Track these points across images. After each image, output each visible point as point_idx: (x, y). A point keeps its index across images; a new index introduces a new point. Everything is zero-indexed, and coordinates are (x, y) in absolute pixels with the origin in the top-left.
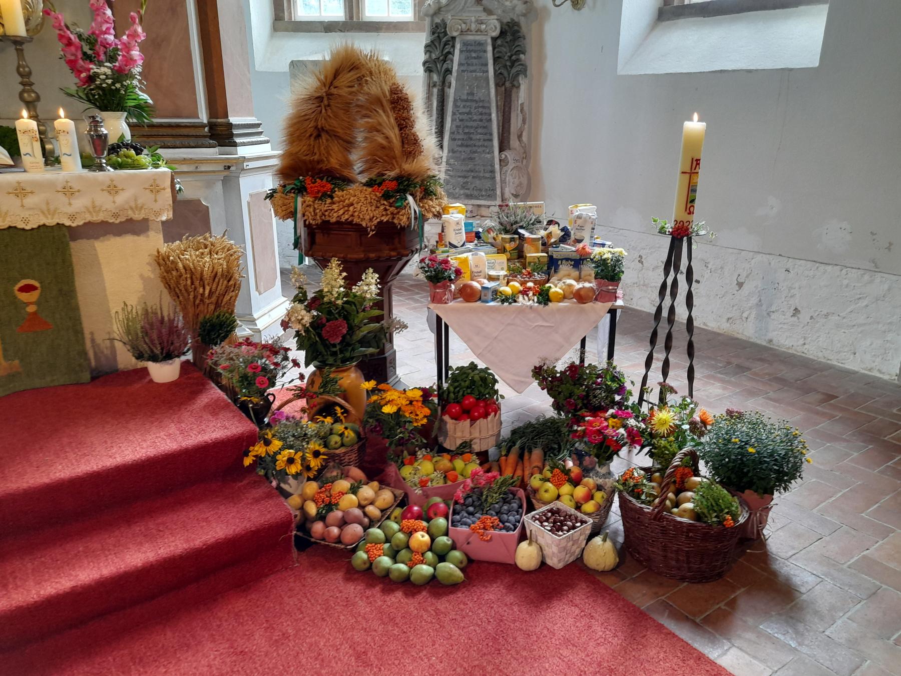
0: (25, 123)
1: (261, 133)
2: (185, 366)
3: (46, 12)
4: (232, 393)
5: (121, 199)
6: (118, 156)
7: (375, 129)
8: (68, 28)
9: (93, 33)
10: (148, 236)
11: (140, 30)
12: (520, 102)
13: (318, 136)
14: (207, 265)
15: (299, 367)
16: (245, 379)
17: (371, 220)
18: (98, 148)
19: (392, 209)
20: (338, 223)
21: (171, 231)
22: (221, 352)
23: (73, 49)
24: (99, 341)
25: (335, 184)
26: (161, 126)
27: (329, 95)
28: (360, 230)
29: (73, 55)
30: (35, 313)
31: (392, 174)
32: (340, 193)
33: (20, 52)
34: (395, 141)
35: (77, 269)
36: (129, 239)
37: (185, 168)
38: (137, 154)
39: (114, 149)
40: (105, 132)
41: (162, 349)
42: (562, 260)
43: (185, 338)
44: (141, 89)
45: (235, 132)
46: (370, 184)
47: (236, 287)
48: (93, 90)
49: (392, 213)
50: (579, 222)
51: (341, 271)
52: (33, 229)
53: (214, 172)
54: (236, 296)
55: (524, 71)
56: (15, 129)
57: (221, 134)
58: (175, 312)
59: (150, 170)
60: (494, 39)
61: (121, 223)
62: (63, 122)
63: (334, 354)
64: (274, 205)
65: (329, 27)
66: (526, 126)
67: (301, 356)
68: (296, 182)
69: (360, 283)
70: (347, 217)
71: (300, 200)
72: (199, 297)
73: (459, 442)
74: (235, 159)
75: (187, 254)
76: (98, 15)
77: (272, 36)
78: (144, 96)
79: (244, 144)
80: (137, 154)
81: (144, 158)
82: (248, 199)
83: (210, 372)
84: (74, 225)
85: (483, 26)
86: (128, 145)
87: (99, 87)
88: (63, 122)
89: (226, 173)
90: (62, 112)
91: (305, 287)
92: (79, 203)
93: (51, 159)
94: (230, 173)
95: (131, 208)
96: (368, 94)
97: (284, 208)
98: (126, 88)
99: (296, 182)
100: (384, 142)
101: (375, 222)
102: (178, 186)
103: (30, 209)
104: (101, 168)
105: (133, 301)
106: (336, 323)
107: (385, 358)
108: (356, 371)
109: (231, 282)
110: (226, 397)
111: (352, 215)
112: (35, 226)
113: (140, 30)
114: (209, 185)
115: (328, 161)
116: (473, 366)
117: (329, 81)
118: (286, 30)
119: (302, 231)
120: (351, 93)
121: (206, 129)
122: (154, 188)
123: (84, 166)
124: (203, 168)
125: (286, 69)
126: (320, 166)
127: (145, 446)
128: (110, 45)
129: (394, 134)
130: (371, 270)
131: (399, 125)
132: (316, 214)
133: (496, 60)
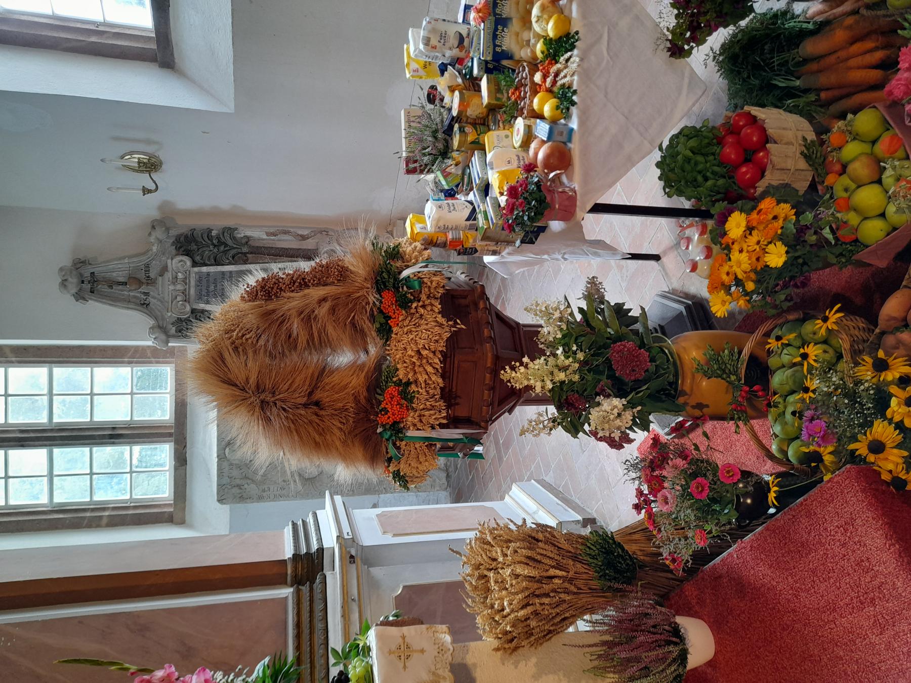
1: (303, 521)
10: (475, 665)
11: (159, 674)
12: (265, 237)
13: (317, 404)
14: (519, 570)
16: (705, 511)
17: (441, 325)
19: (423, 297)
26: (298, 648)
28: (453, 341)
32: (401, 374)
37: (355, 616)
42: (495, 46)
44: (249, 674)
45: (304, 550)
50: (434, 42)
51: (522, 364)
55: (230, 231)
57: (307, 568)
60: (195, 264)
65: (181, 460)
66: (292, 230)
70: (437, 361)
71: (411, 433)
73: (802, 164)
74: (340, 548)
78: (259, 668)
79: (320, 539)
85: (180, 276)
89: (358, 560)
94: (355, 555)
97: (422, 459)
100: (327, 306)
111: (434, 353)
113: (159, 674)
114: (374, 584)
116: (658, 165)
117: (238, 392)
118: (184, 509)
125: (226, 507)
126: (363, 401)
133: (217, 263)
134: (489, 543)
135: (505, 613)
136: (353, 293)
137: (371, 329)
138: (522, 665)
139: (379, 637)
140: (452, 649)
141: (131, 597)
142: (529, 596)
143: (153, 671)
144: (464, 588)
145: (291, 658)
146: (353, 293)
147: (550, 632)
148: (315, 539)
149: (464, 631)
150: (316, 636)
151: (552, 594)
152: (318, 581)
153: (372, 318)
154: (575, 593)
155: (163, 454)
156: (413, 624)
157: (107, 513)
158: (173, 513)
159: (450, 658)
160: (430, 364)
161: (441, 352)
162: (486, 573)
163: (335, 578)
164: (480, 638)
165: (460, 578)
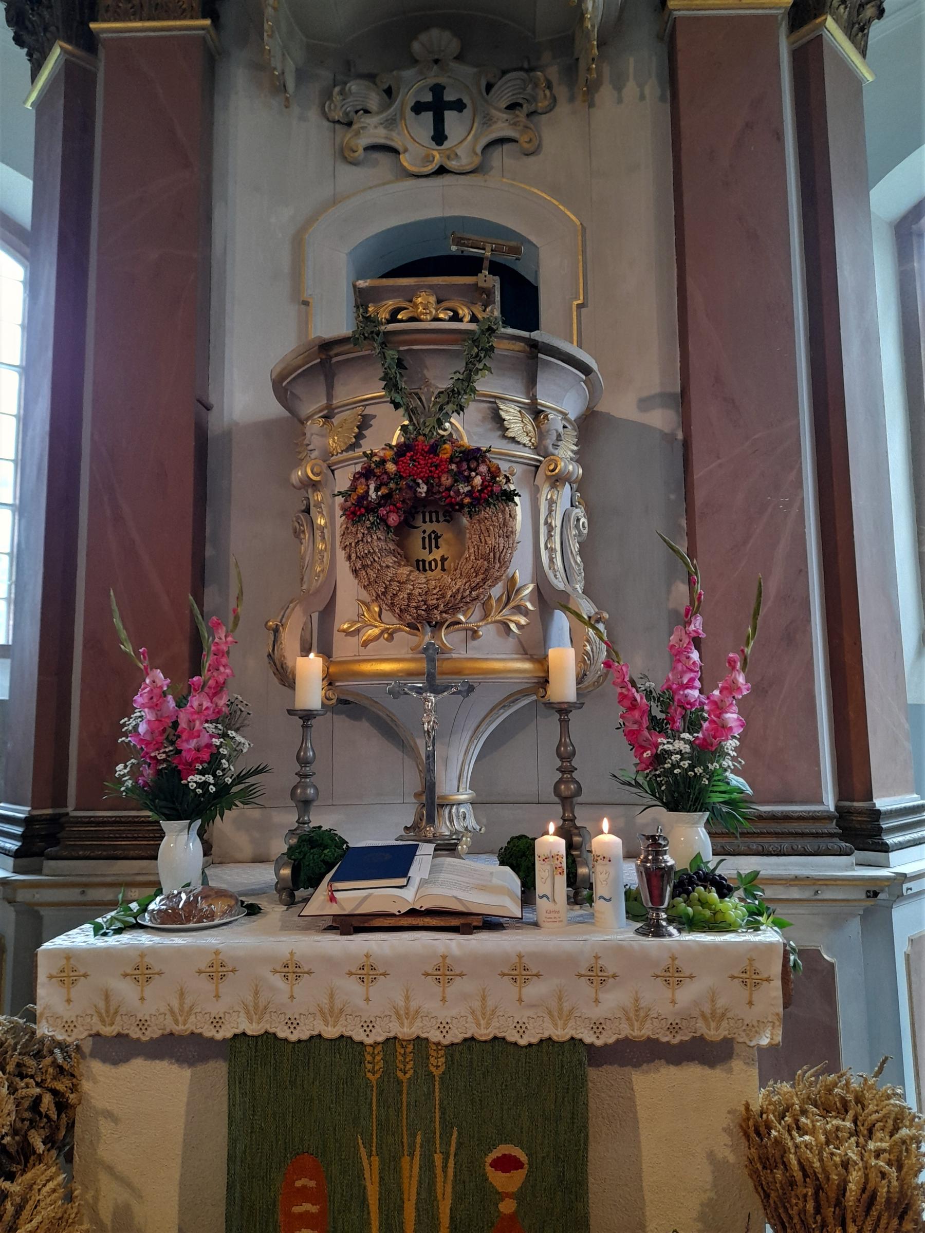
0: (551, 843)
3: (607, 665)
5: (687, 995)
6: (688, 902)
9: (669, 688)
10: (730, 1071)
11: (741, 679)
14: (855, 1176)
18: (656, 892)
23: (637, 714)
29: (635, 722)
30: (513, 1217)
33: (564, 724)
36: (693, 1073)
37: (795, 893)
38: (722, 896)
44: (735, 771)
48: (659, 776)
52: (530, 1045)
53: (847, 900)
74: (887, 879)
76: (679, 661)
78: (737, 781)
79: (901, 846)
80: (722, 896)
84: (599, 1043)
89: (870, 902)
90: (605, 825)
92: (613, 1000)
93: (580, 890)
95: (703, 1015)
98: (711, 774)
103: (532, 1006)
112: (534, 1040)
113: (741, 679)
114: (837, 922)
122: (747, 972)
124: (827, 895)
128: (692, 705)
134: (896, 1129)
135: (795, 1133)
138: (727, 1139)
139: (770, 946)
140: (752, 1044)
141: (796, 101)
142: (817, 1179)
143: (744, 672)
144: (828, 1070)
147: (767, 1196)
148: (900, 839)
149: (775, 1064)
150: (774, 840)
151: (819, 1218)
152: (843, 844)
156: (784, 994)
159: (741, 1040)
162: (851, 1113)
163: (849, 867)
164: (763, 1084)
165: (844, 1069)
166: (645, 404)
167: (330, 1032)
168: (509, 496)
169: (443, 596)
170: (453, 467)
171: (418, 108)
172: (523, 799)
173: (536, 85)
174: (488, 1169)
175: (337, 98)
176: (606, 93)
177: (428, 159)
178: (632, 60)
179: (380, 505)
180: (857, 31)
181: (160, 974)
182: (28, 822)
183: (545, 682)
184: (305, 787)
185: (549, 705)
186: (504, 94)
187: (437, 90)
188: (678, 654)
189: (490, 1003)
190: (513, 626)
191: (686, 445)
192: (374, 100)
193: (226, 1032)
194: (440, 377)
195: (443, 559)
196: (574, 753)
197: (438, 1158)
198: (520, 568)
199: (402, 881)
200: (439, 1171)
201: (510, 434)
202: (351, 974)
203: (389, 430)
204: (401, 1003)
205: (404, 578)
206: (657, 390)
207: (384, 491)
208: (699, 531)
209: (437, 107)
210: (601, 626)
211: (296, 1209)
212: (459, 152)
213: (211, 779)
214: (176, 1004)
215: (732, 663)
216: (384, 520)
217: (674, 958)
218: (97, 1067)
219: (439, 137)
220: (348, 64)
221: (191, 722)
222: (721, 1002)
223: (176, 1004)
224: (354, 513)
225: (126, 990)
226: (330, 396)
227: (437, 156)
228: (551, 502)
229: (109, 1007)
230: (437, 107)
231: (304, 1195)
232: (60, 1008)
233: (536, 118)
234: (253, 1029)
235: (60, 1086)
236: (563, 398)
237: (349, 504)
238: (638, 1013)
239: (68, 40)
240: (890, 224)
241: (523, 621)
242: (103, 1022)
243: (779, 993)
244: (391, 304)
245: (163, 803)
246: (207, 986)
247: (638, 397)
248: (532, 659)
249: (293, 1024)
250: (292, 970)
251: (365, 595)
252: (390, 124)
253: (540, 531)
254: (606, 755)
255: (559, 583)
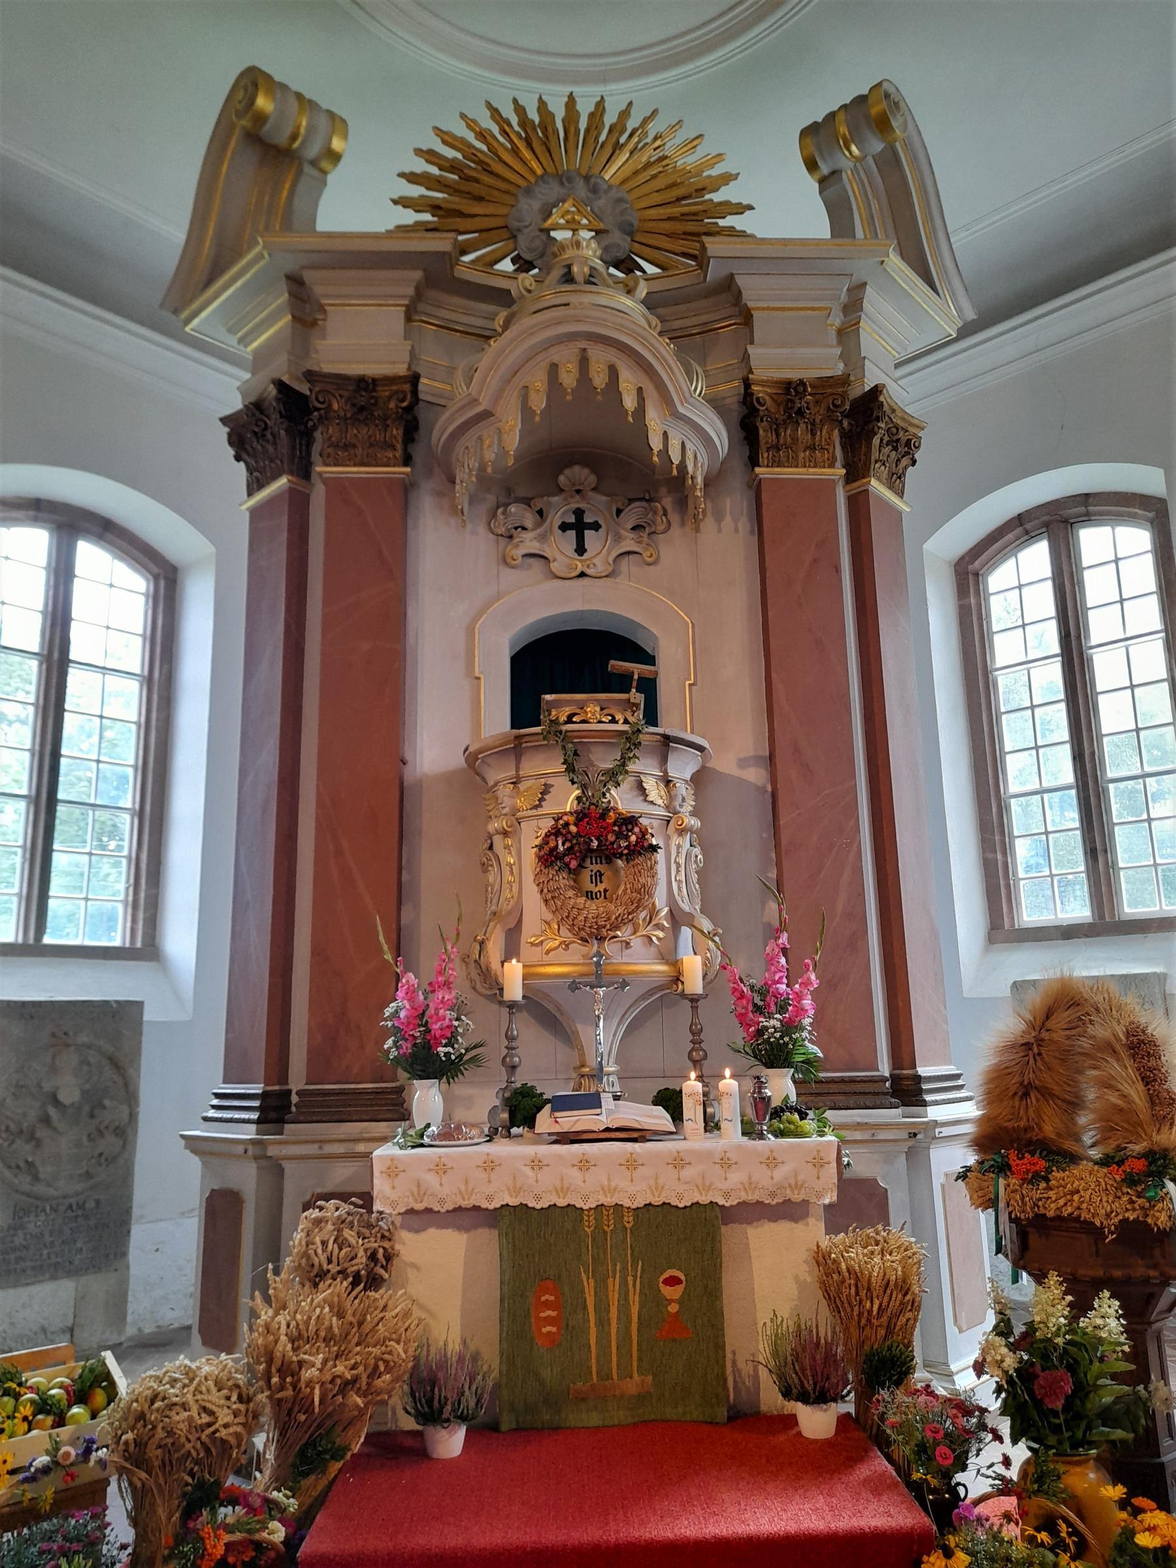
0: (692, 1086)
2: (844, 1421)
4: (904, 1472)
5: (780, 1174)
6: (780, 1121)
7: (1108, 1084)
8: (742, 981)
9: (766, 984)
10: (807, 1224)
13: (1026, 1095)
14: (876, 1269)
15: (1002, 1442)
16: (923, 1451)
17: (1108, 1215)
18: (760, 1113)
19: (1140, 1201)
20: (1058, 1218)
21: (836, 1219)
22: (894, 1405)
23: (744, 1002)
24: (741, 1364)
25: (1053, 1161)
26: (832, 1081)
27: (1040, 1041)
28: (1094, 1231)
31: (1138, 1148)
33: (695, 1009)
34: (1137, 1100)
35: (726, 1260)
37: (858, 1135)
38: (802, 1119)
39: (777, 1113)
40: (769, 1094)
41: (815, 1384)
43: (846, 1374)
44: (811, 1041)
45: (924, 1087)
46: (1105, 1162)
47: (915, 1306)
49: (1142, 1208)
51: (1066, 1293)
52: (686, 1207)
54: (915, 1320)
56: (681, 1091)
57: (908, 1091)
58: (834, 1333)
59: (815, 1138)
61: (777, 1204)
62: (728, 1083)
63: (1056, 1429)
64: (969, 1189)
65: (1069, 933)
67: (1005, 1426)
68: (995, 1157)
69: (1091, 1314)
70: (1070, 1210)
71: (1002, 1182)
72: (866, 1314)
74: (923, 1123)
75: (854, 1251)
77: (986, 950)
78: (814, 1049)
79: (936, 1103)
80: (802, 1119)
81: (809, 1125)
82: (942, 1180)
83: (877, 1435)
84: (727, 1205)
86: (792, 1107)
87: (767, 1041)
88: (728, 1083)
89: (911, 1143)
90: (727, 1072)
91: (1008, 1312)
92: (736, 1178)
93: (711, 1125)
94: (918, 1141)
95: (790, 1186)
96: (1093, 1037)
97: (980, 1193)
99: (995, 1157)
101: (1116, 1220)
102: (846, 1160)
104: (761, 1136)
105: (784, 1312)
106: (1054, 1372)
107: (1162, 1465)
108: (1098, 1469)
109: (908, 1297)
110: (894, 1473)
111: (1079, 1208)
112: (689, 1204)
113: (813, 977)
115: (1040, 1129)
119: (1006, 1227)
120: (1069, 1038)
121: (888, 1084)
122: (818, 1163)
123: (743, 1134)
124: (882, 1135)
125: (1008, 993)
126: (1029, 1135)
127: (784, 1517)
128: (782, 995)
129: (1136, 1093)
130: (1107, 1294)
131: (1143, 1079)
132: (1024, 1204)
136: (1143, 1129)
137: (1109, 1148)
138: (805, 1267)
145: (822, 1075)
146: (1143, 1129)
153: (1119, 1149)
154: (859, 1322)
155: (1077, 909)
157: (999, 856)
158: (1001, 927)
160: (1066, 1204)
161: (1080, 1216)
166: (743, 763)
167: (561, 1203)
168: (654, 849)
169: (609, 919)
170: (616, 828)
171: (564, 527)
172: (651, 1074)
173: (655, 513)
174: (661, 1285)
175: (500, 516)
176: (708, 524)
177: (572, 568)
178: (728, 501)
179: (565, 855)
180: (896, 481)
181: (452, 1168)
182: (264, 1096)
183: (677, 979)
184: (512, 1056)
185: (683, 995)
186: (631, 517)
187: (579, 513)
188: (771, 960)
189: (661, 1182)
190: (654, 939)
191: (774, 795)
192: (529, 520)
193: (496, 1204)
194: (605, 761)
195: (606, 891)
196: (701, 1030)
197: (630, 1279)
198: (660, 899)
199: (598, 1111)
200: (631, 1286)
201: (650, 799)
202: (574, 1166)
203: (566, 799)
204: (606, 1183)
205: (581, 906)
206: (752, 753)
207: (568, 845)
208: (786, 863)
209: (579, 526)
210: (717, 939)
211: (543, 1315)
212: (595, 561)
213: (451, 1050)
214: (463, 1188)
215: (807, 966)
216: (567, 865)
217: (772, 1152)
218: (405, 1235)
219: (581, 550)
220: (509, 491)
221: (437, 1009)
222: (801, 1177)
223: (463, 1188)
224: (547, 860)
225: (431, 1180)
226: (517, 770)
227: (580, 565)
228: (679, 846)
229: (420, 1189)
230: (579, 526)
231: (547, 1305)
232: (388, 1191)
233: (655, 537)
234: (513, 1202)
235: (386, 1244)
236: (682, 767)
237: (542, 853)
238: (750, 1185)
239: (291, 473)
240: (950, 563)
241: (661, 934)
242: (416, 1200)
243: (835, 1170)
244: (568, 710)
245: (419, 1067)
246: (483, 1175)
247: (737, 750)
248: (667, 963)
249: (538, 1198)
250: (536, 1164)
251: (549, 916)
252: (543, 538)
253: (673, 872)
254: (723, 1029)
255: (686, 907)
